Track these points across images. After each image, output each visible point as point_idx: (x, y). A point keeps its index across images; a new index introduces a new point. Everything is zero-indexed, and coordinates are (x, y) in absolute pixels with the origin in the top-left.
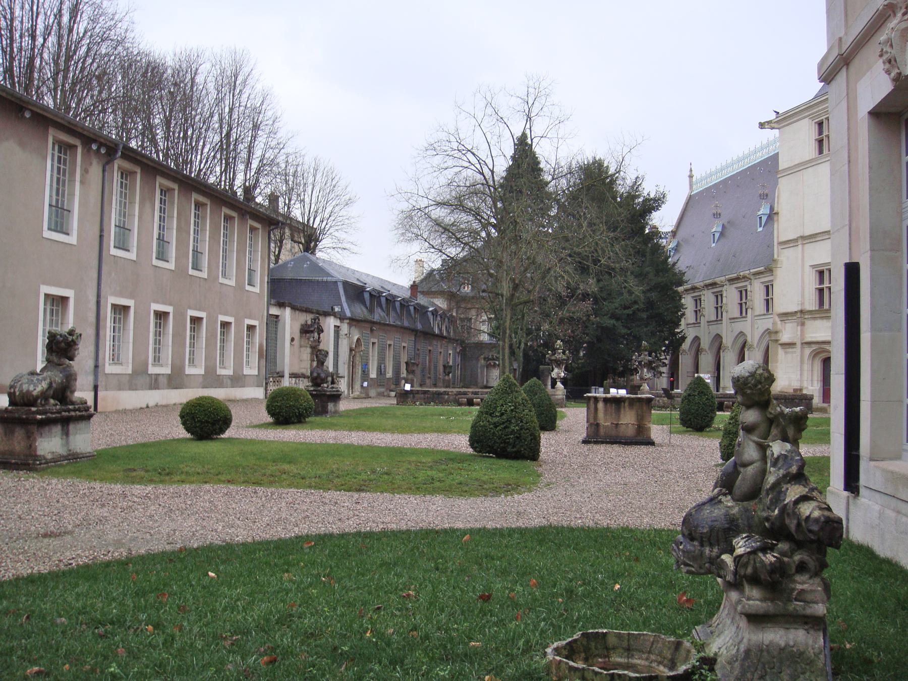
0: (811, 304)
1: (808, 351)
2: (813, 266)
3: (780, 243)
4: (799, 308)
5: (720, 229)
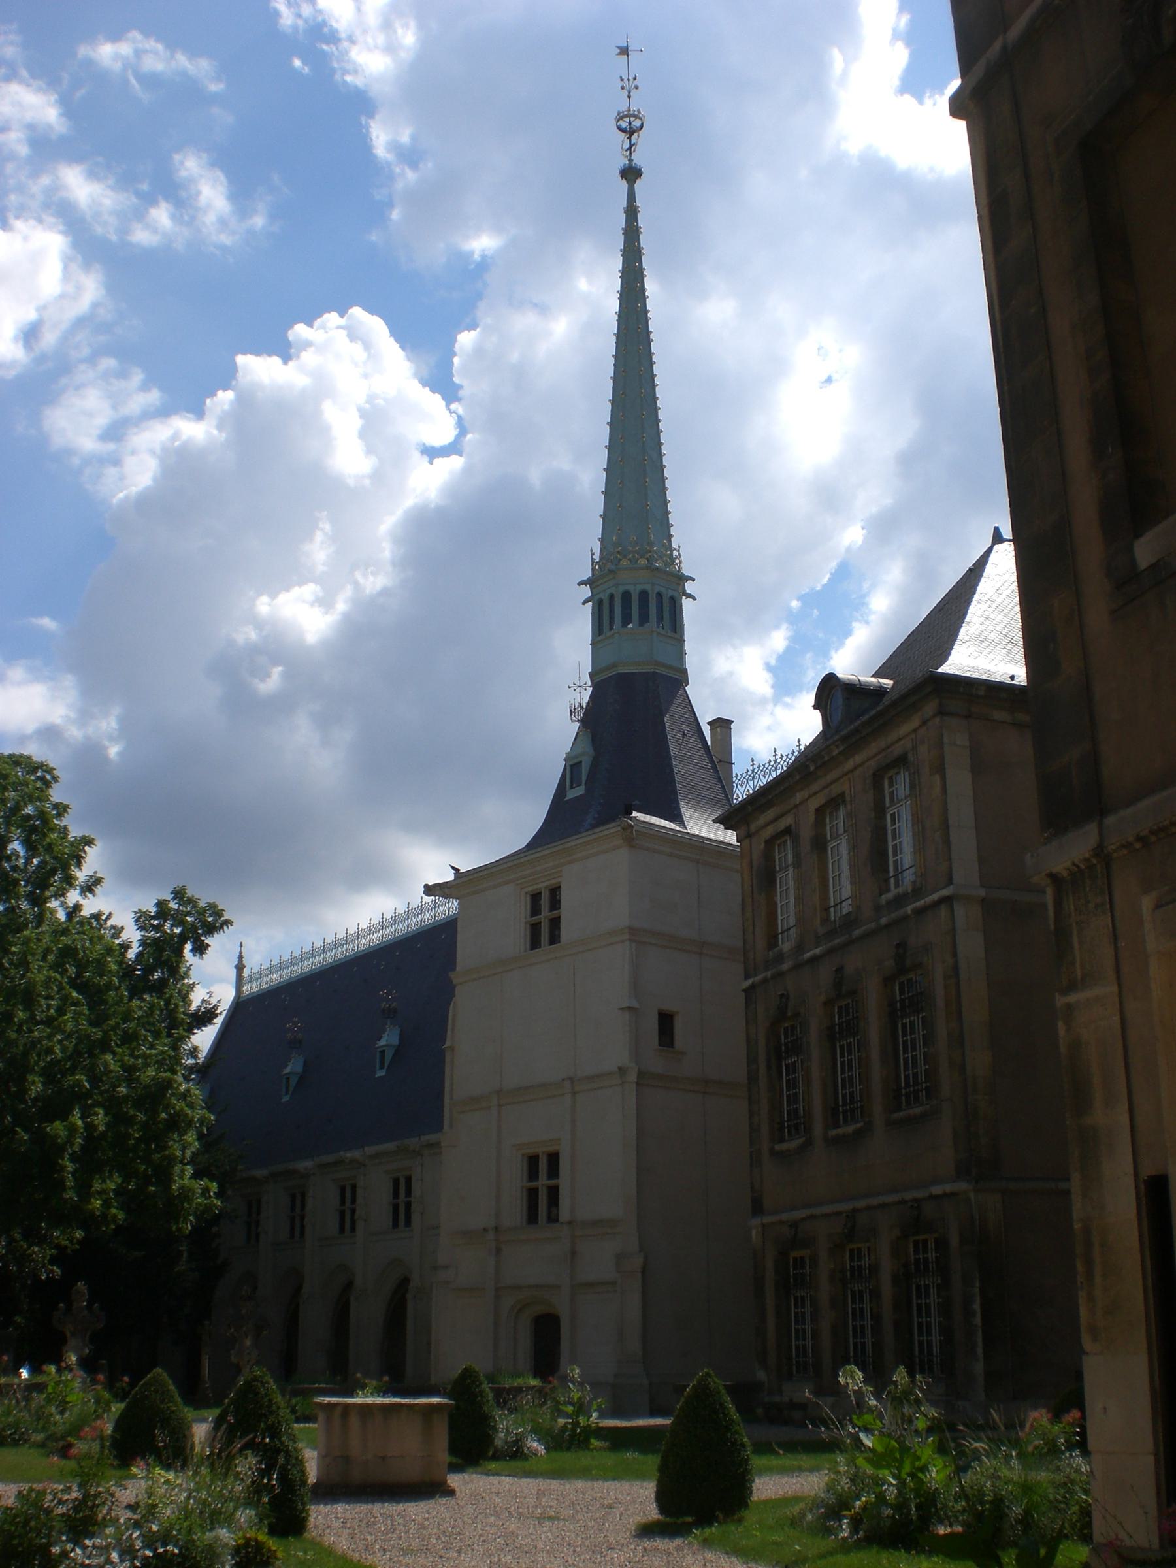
0: (514, 1210)
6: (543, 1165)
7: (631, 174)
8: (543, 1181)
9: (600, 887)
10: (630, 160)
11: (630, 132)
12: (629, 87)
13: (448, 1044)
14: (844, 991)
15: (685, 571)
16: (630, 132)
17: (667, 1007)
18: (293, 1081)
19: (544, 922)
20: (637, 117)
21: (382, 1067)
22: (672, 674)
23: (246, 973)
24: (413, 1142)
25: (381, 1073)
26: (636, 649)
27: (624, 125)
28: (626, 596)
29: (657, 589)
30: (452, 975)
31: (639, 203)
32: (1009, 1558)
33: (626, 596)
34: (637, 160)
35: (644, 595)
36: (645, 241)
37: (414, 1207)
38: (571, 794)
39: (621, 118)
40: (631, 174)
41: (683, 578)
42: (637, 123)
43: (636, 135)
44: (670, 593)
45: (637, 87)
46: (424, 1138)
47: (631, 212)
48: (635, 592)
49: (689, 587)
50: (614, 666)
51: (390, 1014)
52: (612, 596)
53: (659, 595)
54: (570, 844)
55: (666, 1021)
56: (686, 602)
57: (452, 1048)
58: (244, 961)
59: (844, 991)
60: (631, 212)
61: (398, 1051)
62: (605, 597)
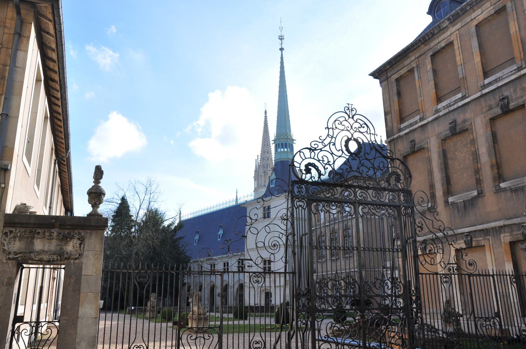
5: (222, 233)
6: (267, 262)
7: (282, 49)
11: (281, 39)
12: (281, 29)
14: (333, 232)
15: (294, 138)
18: (197, 241)
23: (182, 215)
25: (219, 240)
31: (284, 56)
32: (394, 334)
33: (282, 144)
36: (285, 65)
40: (282, 49)
41: (293, 140)
47: (282, 58)
49: (294, 142)
56: (294, 144)
58: (103, 184)
59: (333, 232)
60: (282, 58)
62: (277, 144)
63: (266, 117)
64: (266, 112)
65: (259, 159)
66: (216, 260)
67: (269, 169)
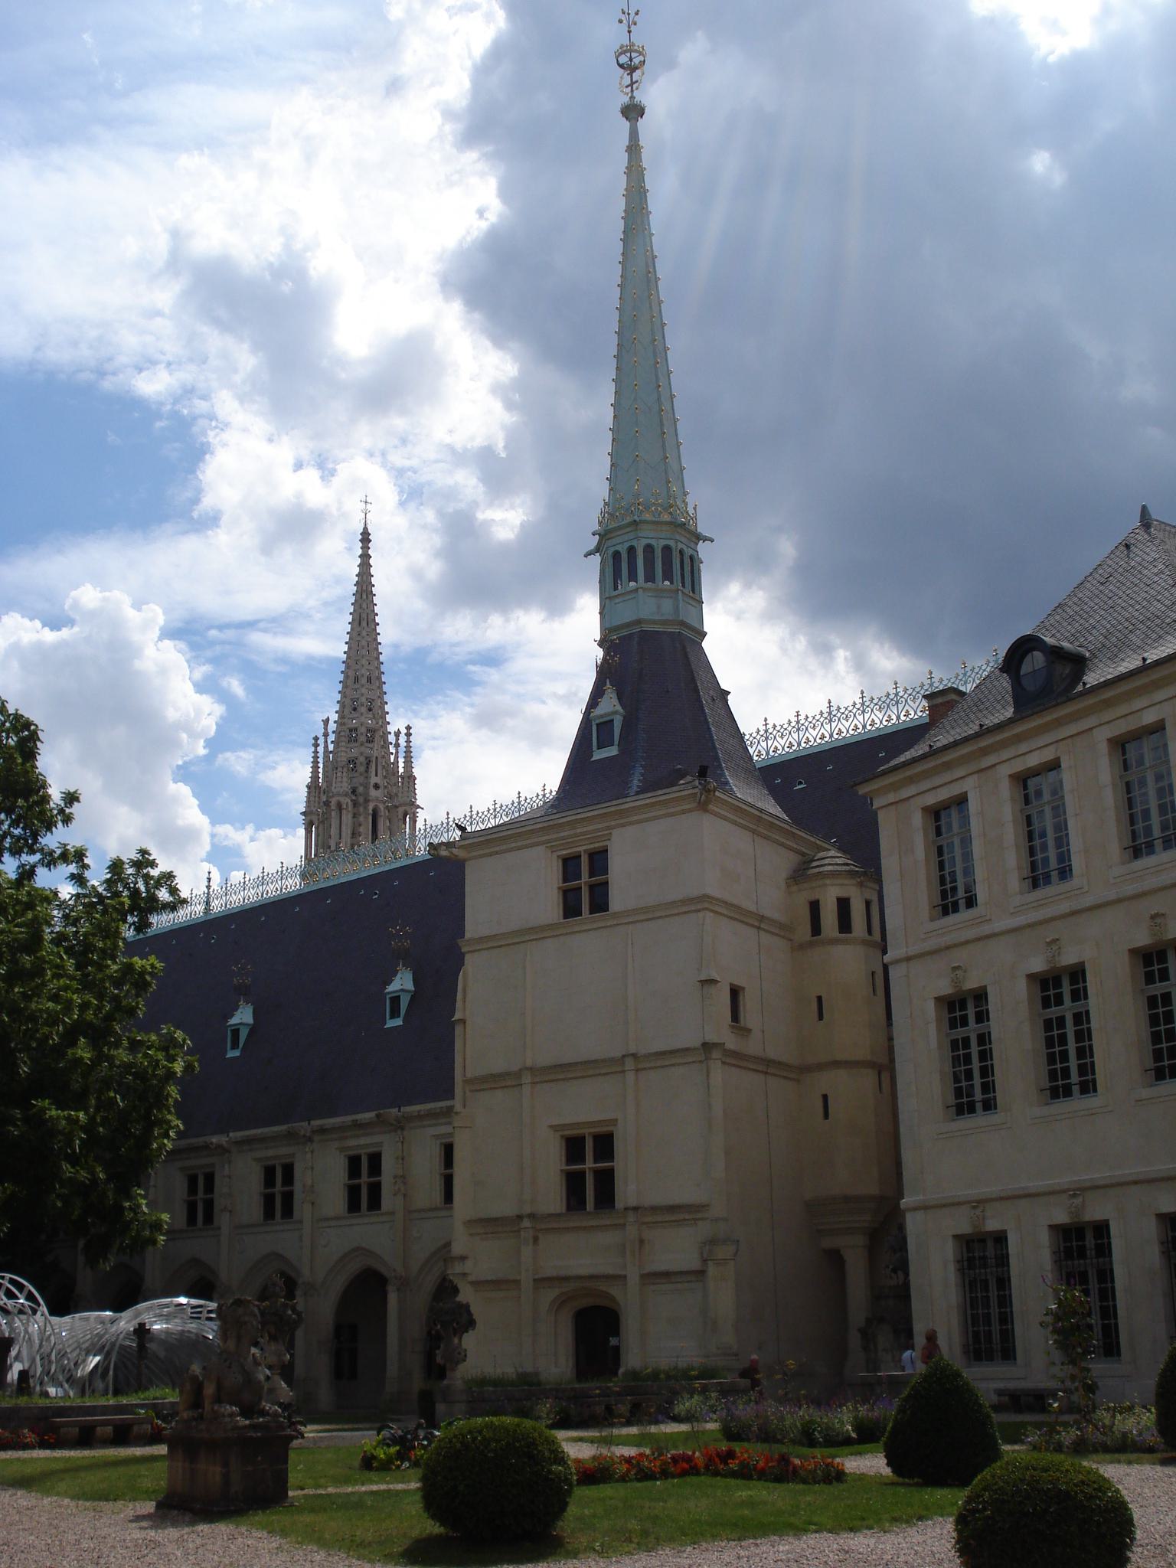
0: (552, 1197)
1: (550, 1295)
2: (554, 1128)
3: (466, 1082)
4: (527, 1210)
8: (364, 1179)
9: (657, 849)
10: (632, 98)
11: (631, 69)
13: (457, 1016)
16: (631, 69)
17: (739, 982)
18: (243, 1034)
19: (585, 888)
20: (641, 53)
21: (235, 1046)
22: (689, 634)
24: (303, 1127)
25: (232, 1054)
26: (648, 606)
27: (623, 59)
28: (649, 549)
29: (680, 546)
30: (460, 942)
33: (649, 549)
34: (640, 97)
35: (667, 549)
37: (298, 1197)
38: (598, 755)
39: (624, 53)
42: (636, 61)
43: (638, 72)
44: (691, 552)
45: (620, 21)
46: (316, 1123)
47: (634, 148)
48: (658, 546)
50: (639, 622)
51: (244, 992)
52: (632, 550)
53: (681, 552)
54: (627, 806)
55: (735, 992)
57: (463, 1021)
60: (634, 148)
61: (253, 1030)
63: (365, 558)
64: (366, 538)
65: (332, 737)
66: (221, 1150)
67: (374, 780)
